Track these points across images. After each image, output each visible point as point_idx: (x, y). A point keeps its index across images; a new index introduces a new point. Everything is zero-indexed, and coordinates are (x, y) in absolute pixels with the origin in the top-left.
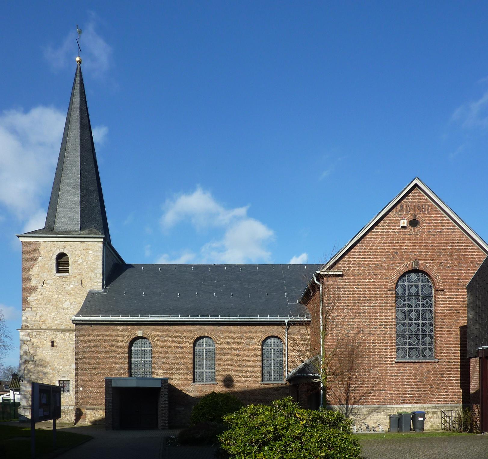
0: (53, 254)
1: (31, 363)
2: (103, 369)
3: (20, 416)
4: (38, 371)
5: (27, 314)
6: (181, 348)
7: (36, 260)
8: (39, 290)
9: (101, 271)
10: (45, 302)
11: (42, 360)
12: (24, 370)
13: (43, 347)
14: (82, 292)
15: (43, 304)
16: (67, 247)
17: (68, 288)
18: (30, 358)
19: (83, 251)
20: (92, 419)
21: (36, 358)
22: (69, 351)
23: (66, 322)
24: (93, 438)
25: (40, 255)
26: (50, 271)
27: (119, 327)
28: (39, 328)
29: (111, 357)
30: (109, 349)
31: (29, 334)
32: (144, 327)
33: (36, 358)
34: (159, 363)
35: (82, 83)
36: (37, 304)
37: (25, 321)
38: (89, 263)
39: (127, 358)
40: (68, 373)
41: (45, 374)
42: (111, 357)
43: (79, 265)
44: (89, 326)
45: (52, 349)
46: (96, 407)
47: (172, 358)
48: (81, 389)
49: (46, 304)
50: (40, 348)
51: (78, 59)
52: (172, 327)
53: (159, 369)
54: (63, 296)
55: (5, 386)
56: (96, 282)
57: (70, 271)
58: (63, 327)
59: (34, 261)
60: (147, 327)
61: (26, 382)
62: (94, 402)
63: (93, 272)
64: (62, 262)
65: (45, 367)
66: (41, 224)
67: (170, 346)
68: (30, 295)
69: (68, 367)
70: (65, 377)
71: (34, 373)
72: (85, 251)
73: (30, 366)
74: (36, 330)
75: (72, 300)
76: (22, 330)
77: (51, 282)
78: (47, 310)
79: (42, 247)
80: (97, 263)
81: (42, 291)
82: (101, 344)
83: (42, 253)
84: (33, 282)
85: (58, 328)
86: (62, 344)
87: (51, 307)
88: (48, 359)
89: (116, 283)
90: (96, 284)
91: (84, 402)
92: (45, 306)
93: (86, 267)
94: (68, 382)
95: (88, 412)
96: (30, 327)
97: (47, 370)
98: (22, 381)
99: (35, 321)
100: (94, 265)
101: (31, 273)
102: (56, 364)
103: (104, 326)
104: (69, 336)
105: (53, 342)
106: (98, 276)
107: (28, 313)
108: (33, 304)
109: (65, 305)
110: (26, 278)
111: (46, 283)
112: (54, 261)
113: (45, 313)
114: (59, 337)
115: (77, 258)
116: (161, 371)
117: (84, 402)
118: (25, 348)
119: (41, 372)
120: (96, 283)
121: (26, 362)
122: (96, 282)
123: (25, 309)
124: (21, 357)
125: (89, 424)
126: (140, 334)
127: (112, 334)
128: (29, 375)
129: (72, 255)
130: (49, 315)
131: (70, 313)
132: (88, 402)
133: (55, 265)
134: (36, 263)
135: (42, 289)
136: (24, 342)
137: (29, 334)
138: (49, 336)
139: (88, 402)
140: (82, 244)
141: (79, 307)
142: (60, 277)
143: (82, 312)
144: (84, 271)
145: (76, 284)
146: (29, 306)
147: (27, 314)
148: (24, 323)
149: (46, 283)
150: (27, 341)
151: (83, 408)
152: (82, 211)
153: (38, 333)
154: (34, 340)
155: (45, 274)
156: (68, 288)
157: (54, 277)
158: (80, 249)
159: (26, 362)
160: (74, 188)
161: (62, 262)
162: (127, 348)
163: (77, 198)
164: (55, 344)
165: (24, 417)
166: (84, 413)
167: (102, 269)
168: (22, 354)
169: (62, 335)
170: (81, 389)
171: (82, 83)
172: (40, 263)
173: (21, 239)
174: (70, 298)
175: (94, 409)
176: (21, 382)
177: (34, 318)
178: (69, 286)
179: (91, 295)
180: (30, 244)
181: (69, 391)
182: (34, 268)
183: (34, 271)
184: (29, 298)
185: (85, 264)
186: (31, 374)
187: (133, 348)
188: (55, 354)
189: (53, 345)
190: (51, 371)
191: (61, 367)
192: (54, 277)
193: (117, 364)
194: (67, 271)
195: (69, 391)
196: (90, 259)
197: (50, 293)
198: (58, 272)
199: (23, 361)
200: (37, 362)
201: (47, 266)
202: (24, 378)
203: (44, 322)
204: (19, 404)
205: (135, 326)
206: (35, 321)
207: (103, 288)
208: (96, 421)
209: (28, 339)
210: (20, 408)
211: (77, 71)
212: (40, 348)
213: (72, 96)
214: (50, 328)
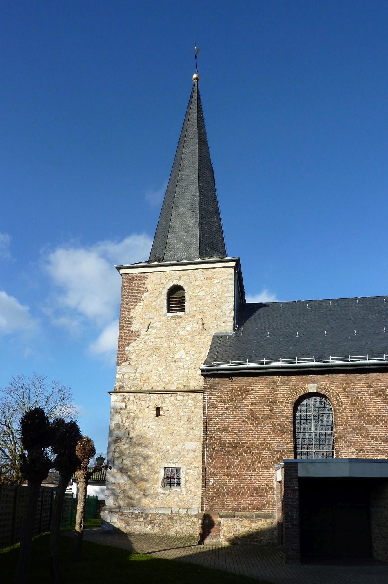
0: (164, 288)
1: (124, 440)
2: (249, 448)
3: (104, 522)
4: (135, 454)
5: (124, 370)
7: (140, 297)
8: (142, 337)
9: (232, 307)
10: (149, 353)
11: (142, 437)
12: (114, 451)
13: (143, 418)
14: (202, 337)
15: (147, 355)
16: (183, 278)
17: (184, 332)
18: (125, 434)
19: (206, 281)
20: (231, 535)
21: (132, 435)
22: (182, 423)
23: (179, 380)
25: (146, 290)
26: (158, 311)
27: (276, 378)
28: (139, 389)
29: (262, 427)
30: (260, 414)
31: (124, 398)
32: (318, 377)
33: (132, 435)
34: (349, 437)
35: (199, 99)
36: (138, 356)
37: (120, 381)
38: (215, 296)
39: (291, 429)
40: (179, 456)
41: (146, 458)
42: (262, 427)
43: (200, 299)
44: (227, 379)
45: (156, 420)
46: (237, 513)
47: (371, 428)
48: (211, 482)
49: (150, 355)
50: (138, 418)
51: (195, 76)
52: (368, 375)
53: (348, 447)
54: (175, 343)
55: (55, 478)
56: (225, 322)
57: (186, 308)
58: (174, 388)
59: (137, 299)
60: (324, 376)
61: (115, 471)
62: (234, 504)
63: (219, 307)
64: (176, 299)
65: (146, 447)
66: (145, 254)
67: (367, 407)
68: (129, 343)
69: (179, 447)
70: (173, 462)
71: (129, 457)
72: (209, 281)
73: (124, 446)
74: (134, 393)
75: (187, 349)
76: (115, 392)
77: (159, 325)
78: (152, 364)
79: (149, 280)
80: (227, 295)
81: (146, 338)
82: (246, 406)
83: (149, 288)
84: (135, 327)
85: (167, 388)
86: (171, 412)
87: (158, 359)
88: (149, 435)
89: (248, 324)
90: (224, 324)
91: (216, 504)
92: (149, 359)
93: (209, 301)
95: (223, 521)
96: (127, 389)
97: (148, 452)
98: (111, 468)
99: (133, 380)
100: (222, 298)
101: (131, 315)
102: (162, 443)
103: (252, 379)
104: (182, 400)
105: (158, 410)
106: (228, 312)
107: (125, 368)
108: (132, 357)
109: (178, 356)
111: (152, 327)
112: (165, 297)
113: (149, 368)
114: (167, 402)
115: (197, 291)
117: (216, 504)
118: (118, 419)
119: (139, 454)
120: (225, 323)
121: (118, 439)
122: (225, 322)
123: (121, 363)
124: (111, 432)
125: (225, 543)
126: (312, 388)
127: (265, 389)
128: (120, 460)
129: (190, 287)
130: (154, 371)
131: (185, 366)
132: (223, 505)
133: (165, 302)
134: (140, 301)
135: (146, 335)
136: (117, 411)
137: (124, 398)
138: (154, 400)
139: (223, 505)
140: (205, 272)
141: (205, 353)
142: (172, 317)
143: (210, 359)
144: (206, 308)
145: (195, 325)
146: (127, 359)
147: (124, 370)
148: (118, 384)
149: (152, 327)
150: (121, 409)
151: (216, 515)
152: (201, 235)
153: (137, 396)
154: (132, 407)
155: (152, 315)
156: (184, 332)
157: (163, 318)
158: (202, 278)
159: (118, 439)
160: (190, 209)
161: (176, 299)
162: (291, 412)
163: (195, 220)
164: (161, 412)
165: (109, 524)
166: (217, 523)
167: (233, 303)
168: (112, 428)
169: (173, 398)
170: (211, 482)
171: (199, 99)
172: (145, 301)
173: (122, 271)
174: (186, 345)
175: (233, 517)
176: (109, 470)
177: (133, 375)
178: (184, 328)
179: (218, 340)
180: (133, 277)
181: (178, 484)
182: (137, 307)
183: (137, 311)
184: (127, 348)
185: (208, 297)
186: (123, 457)
187: (298, 413)
188: (161, 427)
189: (158, 414)
190: (153, 453)
191: (168, 447)
192: (163, 318)
193: (274, 439)
195: (178, 484)
197: (158, 340)
198: (169, 311)
199: (114, 438)
200: (134, 440)
201: (154, 303)
202: (113, 464)
203: (146, 381)
204: (103, 503)
205: (304, 377)
206: (133, 380)
207: (234, 329)
208: (237, 538)
209: (123, 405)
210: (105, 510)
211: (194, 88)
212: (138, 418)
213: (187, 113)
214: (155, 388)
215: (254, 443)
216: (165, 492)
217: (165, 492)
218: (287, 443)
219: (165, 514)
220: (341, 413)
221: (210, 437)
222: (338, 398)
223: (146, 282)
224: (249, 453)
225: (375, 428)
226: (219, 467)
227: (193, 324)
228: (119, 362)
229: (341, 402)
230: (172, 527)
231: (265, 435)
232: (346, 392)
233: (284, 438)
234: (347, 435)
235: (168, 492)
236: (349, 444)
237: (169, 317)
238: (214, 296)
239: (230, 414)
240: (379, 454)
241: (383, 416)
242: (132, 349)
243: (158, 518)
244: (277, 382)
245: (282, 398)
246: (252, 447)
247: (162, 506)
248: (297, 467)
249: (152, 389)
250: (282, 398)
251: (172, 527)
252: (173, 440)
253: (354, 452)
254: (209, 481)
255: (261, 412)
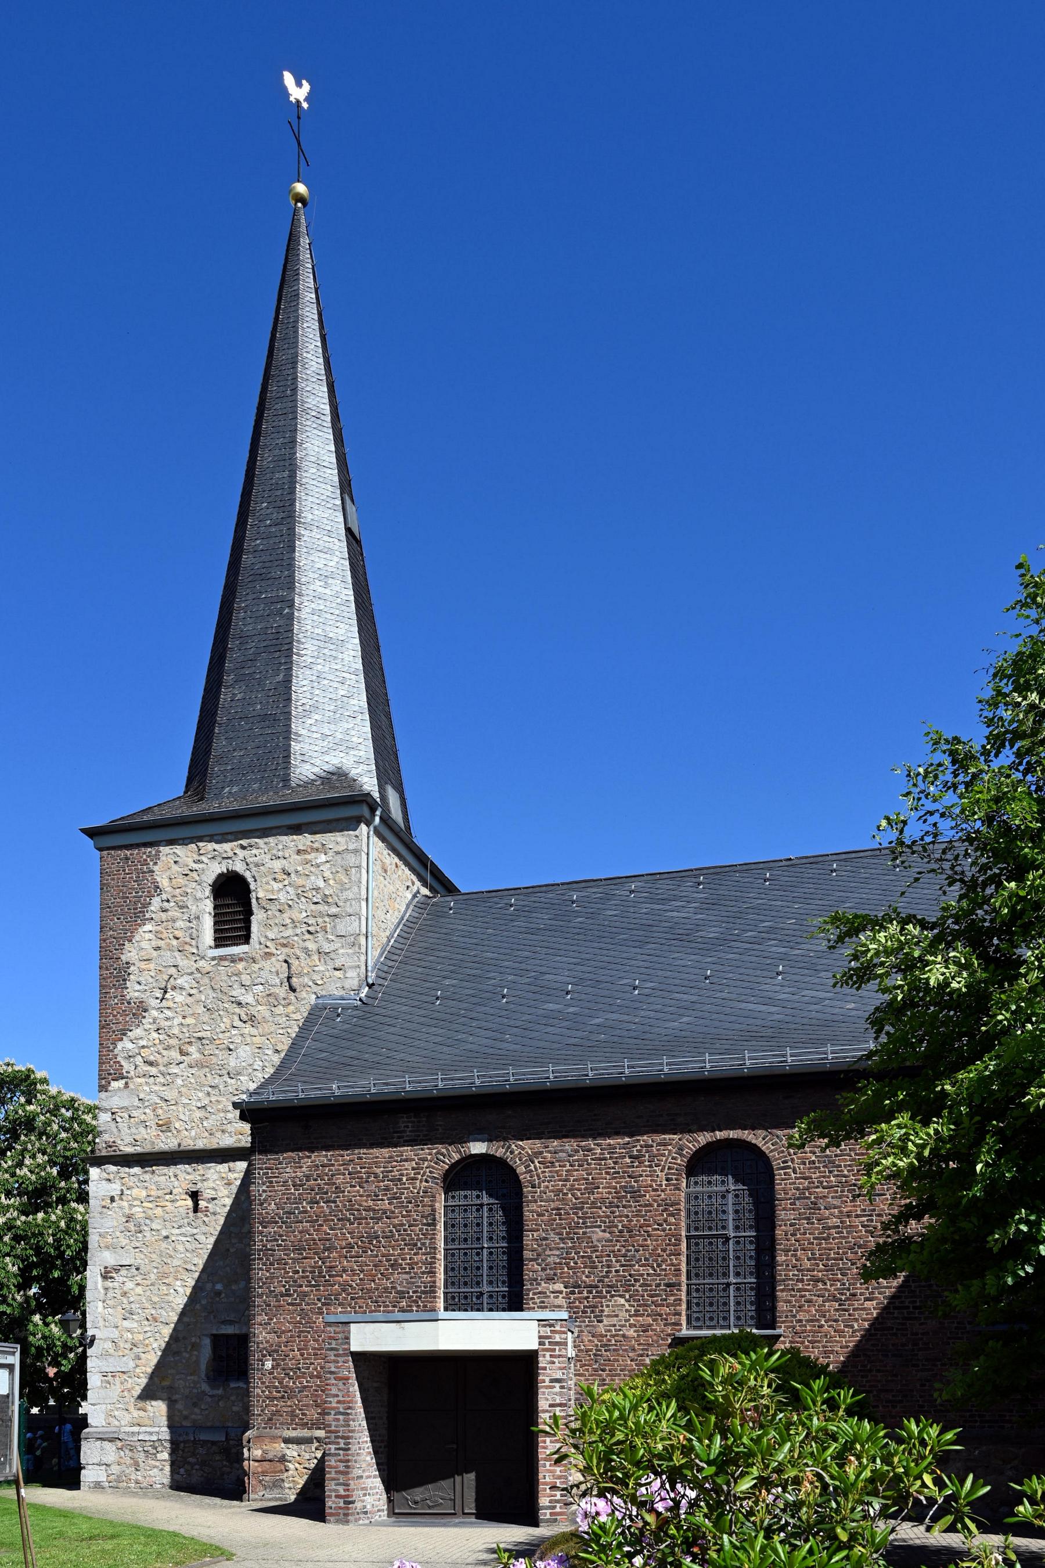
6: (636, 1194)
24: (229, 1556)
28: (148, 1148)
30: (368, 1209)
47: (598, 1234)
53: (550, 1279)
70: (231, 1323)
83: (164, 882)
84: (133, 991)
90: (337, 973)
94: (446, 1309)
105: (195, 1196)
110: (113, 974)
111: (174, 988)
116: (559, 1286)
164: (202, 1204)
174: (254, 1031)
183: (141, 947)
191: (219, 1287)
194: (246, 939)
196: (321, 884)
215: (354, 1275)
216: (216, 1392)
217: (216, 1392)
218: (423, 1273)
219: (213, 1443)
220: (536, 1201)
221: (264, 1264)
222: (532, 1167)
223: (156, 868)
224: (345, 1299)
225: (607, 1235)
226: (283, 1332)
227: (271, 970)
228: (103, 1082)
229: (538, 1176)
230: (228, 1470)
231: (377, 1256)
232: (549, 1152)
233: (417, 1263)
234: (548, 1252)
235: (220, 1392)
236: (552, 1272)
237: (213, 959)
238: (315, 900)
239: (306, 1212)
240: (612, 1296)
241: (624, 1207)
242: (130, 1046)
243: (200, 1450)
244: (405, 1131)
245: (413, 1169)
246: (351, 1286)
247: (209, 1424)
248: (349, 1332)
249: (179, 1145)
250: (413, 1169)
251: (228, 1470)
252: (228, 1269)
253: (561, 1292)
254: (263, 1365)
255: (371, 1203)
